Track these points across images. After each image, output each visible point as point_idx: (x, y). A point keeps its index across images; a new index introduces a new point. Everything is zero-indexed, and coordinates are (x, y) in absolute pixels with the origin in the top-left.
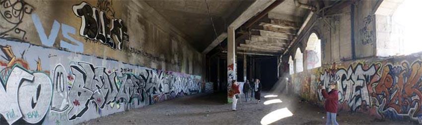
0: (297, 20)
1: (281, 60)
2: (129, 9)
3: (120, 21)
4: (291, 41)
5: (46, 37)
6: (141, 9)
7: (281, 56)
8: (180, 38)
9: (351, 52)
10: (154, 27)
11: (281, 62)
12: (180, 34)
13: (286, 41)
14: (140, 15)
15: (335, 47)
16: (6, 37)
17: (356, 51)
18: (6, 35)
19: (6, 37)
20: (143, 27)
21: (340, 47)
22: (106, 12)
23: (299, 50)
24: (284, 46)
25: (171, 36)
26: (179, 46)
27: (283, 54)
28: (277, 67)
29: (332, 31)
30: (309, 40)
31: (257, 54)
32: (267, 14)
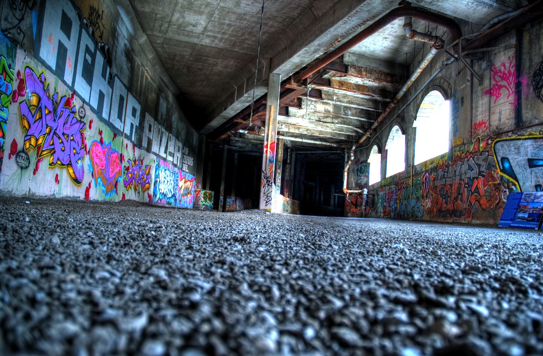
0: (398, 72)
1: (352, 154)
2: (118, 32)
3: (107, 47)
4: (378, 114)
5: (62, 41)
6: (131, 34)
7: (354, 148)
8: (171, 98)
9: (513, 115)
10: (141, 68)
11: (352, 158)
12: (171, 88)
13: (367, 114)
14: (128, 45)
15: (480, 109)
16: (9, 35)
17: (524, 111)
18: (10, 33)
19: (9, 35)
20: (130, 64)
21: (490, 108)
22: (95, 29)
23: (375, 148)
24: (362, 126)
25: (160, 91)
26: (168, 110)
27: (357, 142)
28: (344, 169)
29: (476, 81)
30: (422, 106)
31: (304, 141)
32: (342, 56)
